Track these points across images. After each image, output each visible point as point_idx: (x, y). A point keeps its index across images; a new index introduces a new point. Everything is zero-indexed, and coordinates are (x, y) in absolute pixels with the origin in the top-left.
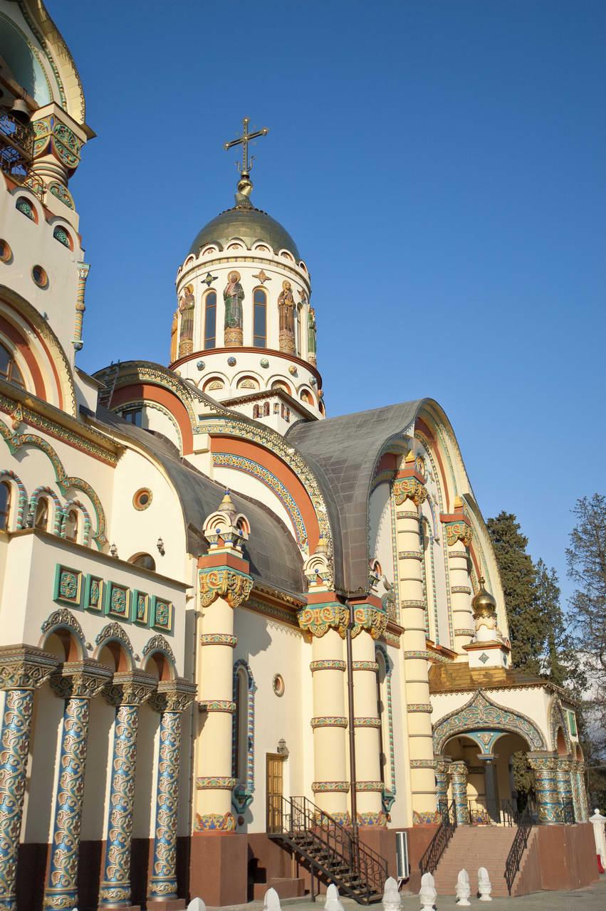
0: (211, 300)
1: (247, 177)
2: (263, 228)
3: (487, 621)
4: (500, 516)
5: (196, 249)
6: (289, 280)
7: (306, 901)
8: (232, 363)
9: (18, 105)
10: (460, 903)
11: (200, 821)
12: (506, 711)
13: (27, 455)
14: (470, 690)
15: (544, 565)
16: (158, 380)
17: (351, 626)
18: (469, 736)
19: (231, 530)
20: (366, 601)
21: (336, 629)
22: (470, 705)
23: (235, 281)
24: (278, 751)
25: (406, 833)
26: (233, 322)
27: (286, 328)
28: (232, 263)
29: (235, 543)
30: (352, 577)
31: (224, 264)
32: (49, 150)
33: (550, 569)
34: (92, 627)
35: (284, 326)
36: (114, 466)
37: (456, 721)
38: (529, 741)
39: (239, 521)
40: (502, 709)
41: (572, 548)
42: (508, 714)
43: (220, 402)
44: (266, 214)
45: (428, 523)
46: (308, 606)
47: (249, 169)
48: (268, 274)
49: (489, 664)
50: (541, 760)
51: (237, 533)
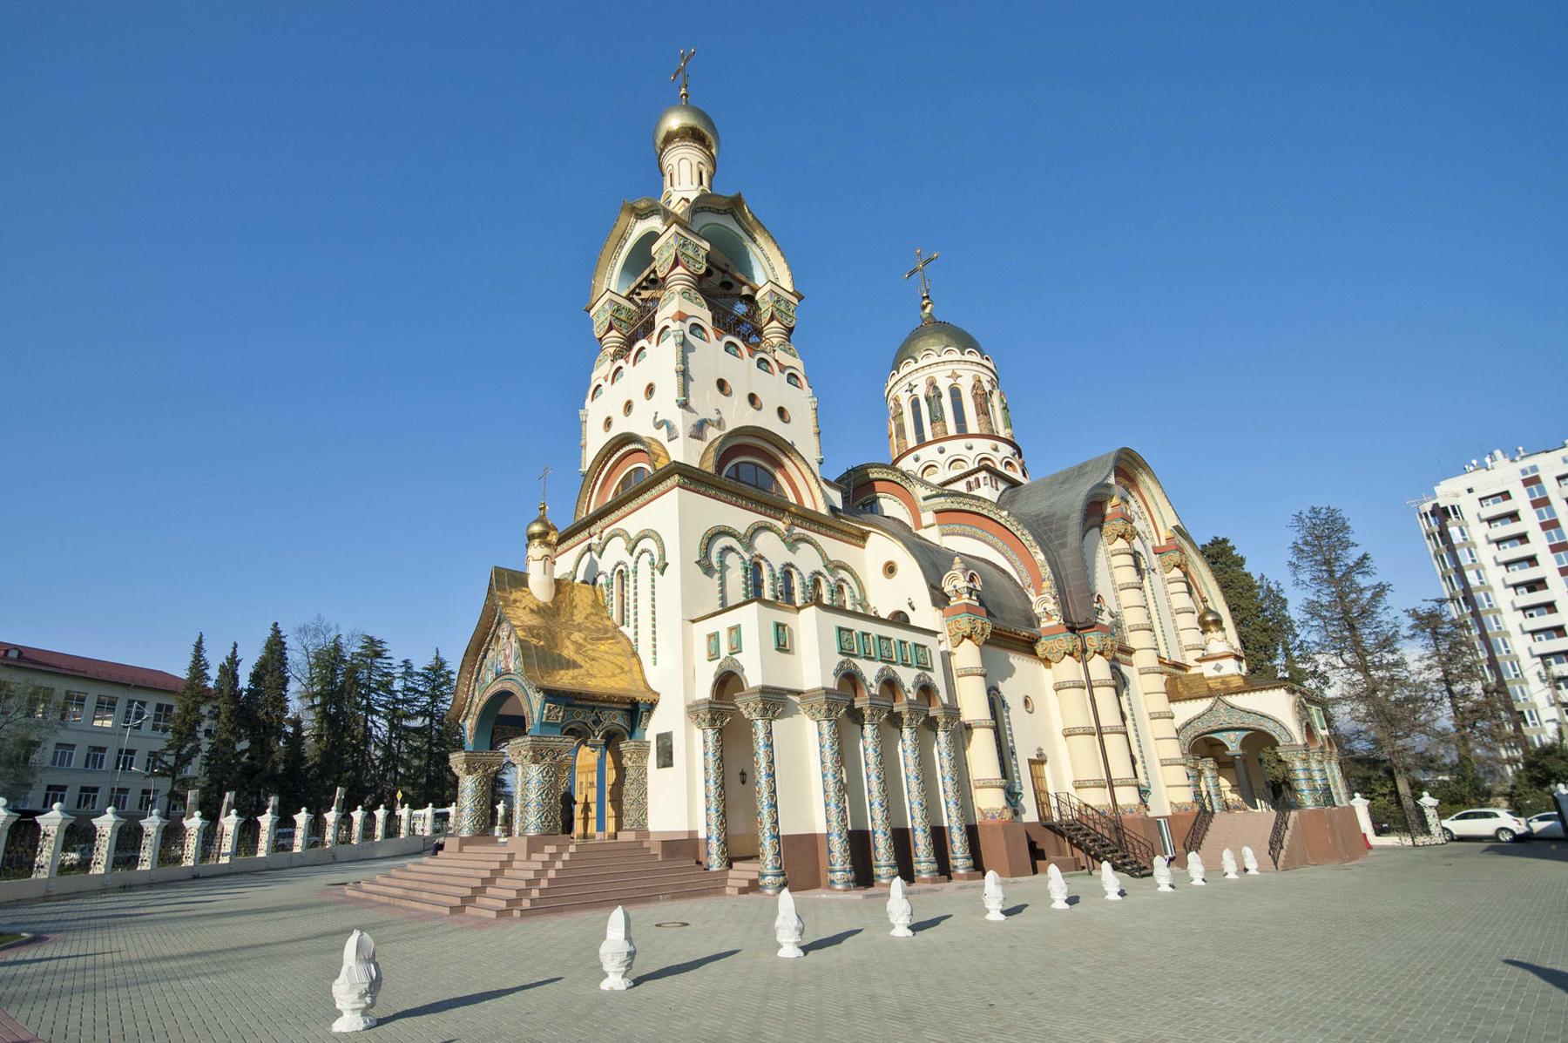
0: (915, 404)
1: (928, 297)
3: (1215, 635)
5: (896, 366)
8: (942, 451)
9: (745, 291)
11: (982, 812)
16: (885, 476)
17: (1085, 651)
18: (1213, 736)
19: (965, 584)
21: (1071, 654)
22: (1211, 709)
23: (932, 385)
26: (937, 418)
28: (928, 370)
29: (971, 594)
31: (921, 373)
32: (772, 318)
34: (870, 671)
36: (864, 547)
41: (1294, 560)
47: (928, 291)
48: (959, 373)
49: (1223, 673)
51: (971, 586)
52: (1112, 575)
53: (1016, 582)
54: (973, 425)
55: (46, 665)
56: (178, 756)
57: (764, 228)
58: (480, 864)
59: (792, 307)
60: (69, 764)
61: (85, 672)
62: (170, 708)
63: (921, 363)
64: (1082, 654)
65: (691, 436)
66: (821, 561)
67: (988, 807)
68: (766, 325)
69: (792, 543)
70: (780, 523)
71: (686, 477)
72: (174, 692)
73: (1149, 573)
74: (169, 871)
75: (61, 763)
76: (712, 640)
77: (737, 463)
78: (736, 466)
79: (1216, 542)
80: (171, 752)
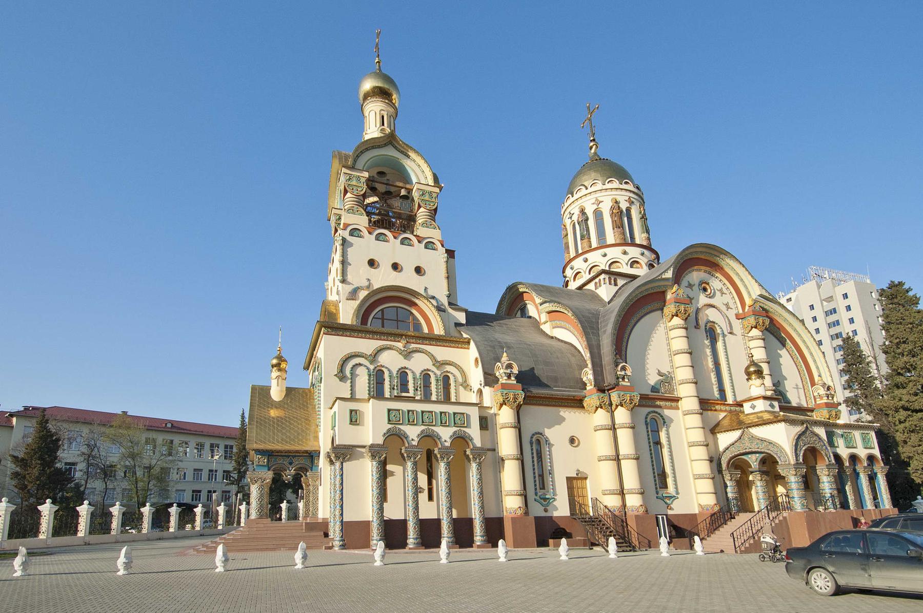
1: (594, 140)
2: (595, 171)
3: (755, 381)
4: (889, 285)
6: (614, 196)
7: (587, 549)
8: (586, 260)
9: (403, 192)
13: (413, 357)
19: (824, 392)
20: (615, 390)
23: (583, 212)
25: (665, 516)
26: (586, 236)
27: (616, 227)
29: (828, 397)
30: (608, 377)
35: (615, 226)
36: (469, 349)
40: (758, 439)
43: (576, 289)
44: (607, 159)
45: (717, 324)
46: (586, 398)
48: (600, 199)
49: (756, 410)
50: (786, 470)
51: (828, 393)
52: (669, 344)
53: (583, 357)
54: (611, 238)
55: (184, 430)
56: (239, 472)
57: (414, 150)
59: (434, 195)
60: (201, 479)
61: (202, 432)
62: (231, 447)
63: (576, 197)
64: (610, 407)
65: (347, 299)
66: (431, 362)
67: (705, 504)
68: (417, 212)
69: (407, 355)
70: (399, 344)
71: (328, 327)
72: (235, 439)
73: (724, 336)
74: (182, 533)
75: (198, 479)
76: (484, 426)
77: (382, 309)
78: (382, 310)
79: (892, 286)
80: (235, 472)
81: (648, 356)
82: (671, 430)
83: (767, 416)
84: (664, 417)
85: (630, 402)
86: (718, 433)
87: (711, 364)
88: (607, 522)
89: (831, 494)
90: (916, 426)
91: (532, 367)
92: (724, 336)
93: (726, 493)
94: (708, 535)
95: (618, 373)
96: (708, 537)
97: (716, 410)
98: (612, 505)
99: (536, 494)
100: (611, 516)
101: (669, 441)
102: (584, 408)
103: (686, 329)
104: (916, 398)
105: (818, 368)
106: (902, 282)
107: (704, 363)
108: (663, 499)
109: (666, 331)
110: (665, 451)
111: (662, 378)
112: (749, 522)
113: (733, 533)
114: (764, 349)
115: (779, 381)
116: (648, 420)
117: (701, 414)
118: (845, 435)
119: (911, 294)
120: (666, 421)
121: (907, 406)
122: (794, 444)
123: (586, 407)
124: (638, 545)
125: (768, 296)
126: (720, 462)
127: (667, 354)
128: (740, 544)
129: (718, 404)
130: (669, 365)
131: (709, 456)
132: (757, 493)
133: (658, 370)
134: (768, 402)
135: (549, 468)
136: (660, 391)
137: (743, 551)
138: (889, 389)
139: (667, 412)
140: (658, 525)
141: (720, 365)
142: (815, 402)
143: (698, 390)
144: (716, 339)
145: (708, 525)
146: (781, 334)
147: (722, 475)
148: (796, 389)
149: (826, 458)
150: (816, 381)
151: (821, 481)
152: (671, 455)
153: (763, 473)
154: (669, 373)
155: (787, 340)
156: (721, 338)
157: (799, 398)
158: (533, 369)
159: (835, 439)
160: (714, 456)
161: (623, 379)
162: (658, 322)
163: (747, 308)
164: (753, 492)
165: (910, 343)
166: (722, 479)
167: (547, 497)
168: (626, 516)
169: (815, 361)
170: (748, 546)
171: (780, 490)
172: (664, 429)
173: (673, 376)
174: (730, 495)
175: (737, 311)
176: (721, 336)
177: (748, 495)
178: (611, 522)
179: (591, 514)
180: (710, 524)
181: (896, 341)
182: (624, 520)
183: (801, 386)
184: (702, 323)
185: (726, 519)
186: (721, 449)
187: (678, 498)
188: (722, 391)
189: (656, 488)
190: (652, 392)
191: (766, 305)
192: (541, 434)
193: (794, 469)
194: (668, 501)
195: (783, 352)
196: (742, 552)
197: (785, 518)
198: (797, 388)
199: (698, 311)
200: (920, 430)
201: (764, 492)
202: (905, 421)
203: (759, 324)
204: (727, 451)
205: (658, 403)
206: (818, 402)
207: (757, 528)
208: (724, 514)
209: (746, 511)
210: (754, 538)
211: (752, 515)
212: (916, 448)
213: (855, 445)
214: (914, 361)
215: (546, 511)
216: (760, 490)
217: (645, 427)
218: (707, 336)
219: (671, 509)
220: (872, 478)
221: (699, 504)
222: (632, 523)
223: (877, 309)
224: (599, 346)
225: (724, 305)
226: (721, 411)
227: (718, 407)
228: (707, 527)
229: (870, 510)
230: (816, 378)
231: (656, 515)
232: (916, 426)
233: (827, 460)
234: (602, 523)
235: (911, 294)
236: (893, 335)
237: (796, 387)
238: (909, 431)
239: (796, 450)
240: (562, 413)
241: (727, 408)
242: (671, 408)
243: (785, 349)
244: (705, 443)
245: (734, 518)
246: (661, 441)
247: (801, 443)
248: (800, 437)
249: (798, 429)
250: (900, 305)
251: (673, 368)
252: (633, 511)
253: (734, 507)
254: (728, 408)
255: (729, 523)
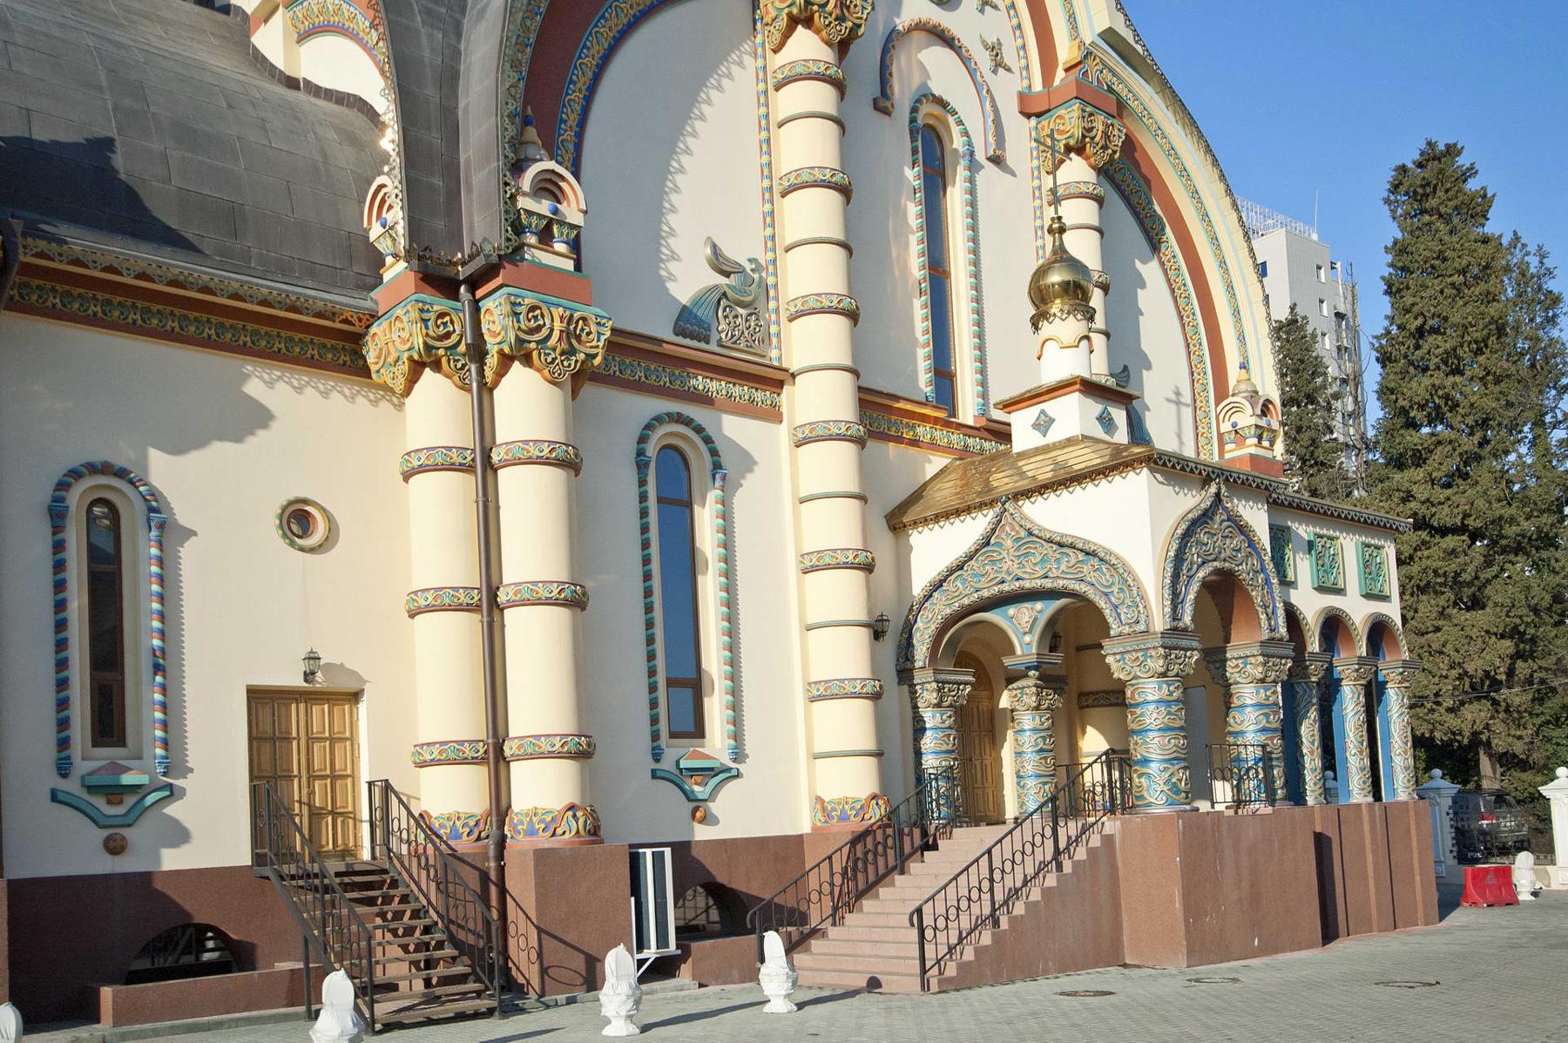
3: (1064, 327)
4: (1422, 154)
10: (608, 1031)
12: (1061, 545)
14: (981, 506)
15: (1524, 245)
19: (1253, 421)
22: (986, 542)
24: (306, 681)
25: (668, 851)
29: (1260, 438)
30: (476, 220)
33: (1532, 248)
37: (959, 585)
38: (1107, 612)
39: (1264, 405)
40: (1050, 541)
42: (1064, 550)
45: (954, 113)
49: (1056, 434)
50: (1135, 655)
51: (1263, 423)
58: (881, 920)
73: (974, 167)
81: (679, 178)
82: (739, 501)
83: (1083, 458)
84: (719, 445)
85: (564, 346)
86: (915, 524)
87: (915, 264)
88: (417, 884)
89: (1264, 747)
90: (1435, 571)
91: (99, 131)
92: (974, 167)
93: (918, 754)
94: (833, 915)
95: (520, 205)
96: (834, 924)
97: (915, 443)
98: (449, 809)
99: (64, 769)
100: (431, 862)
101: (728, 545)
102: (365, 372)
103: (839, 85)
104: (1448, 492)
105: (1241, 339)
106: (1455, 144)
107: (894, 254)
108: (678, 779)
109: (762, 86)
110: (709, 587)
111: (722, 280)
112: (984, 861)
113: (919, 911)
114: (1096, 235)
115: (1125, 368)
116: (651, 450)
117: (860, 442)
118: (1319, 544)
119: (1473, 185)
120: (725, 459)
121: (1424, 517)
122: (1172, 554)
123: (373, 368)
124: (535, 982)
125: (1131, 41)
126: (910, 636)
127: (757, 184)
128: (943, 950)
129: (924, 418)
130: (759, 233)
131: (870, 611)
132: (1019, 754)
133: (714, 246)
134: (1095, 407)
135: (156, 642)
136: (714, 337)
137: (950, 980)
138: (1372, 479)
139: (734, 429)
140: (636, 888)
141: (947, 275)
142: (1221, 452)
143: (857, 346)
144: (943, 176)
145: (838, 880)
146: (1150, 203)
147: (912, 686)
148: (1173, 407)
149: (1263, 617)
150: (1232, 382)
151: (1236, 702)
152: (731, 603)
153: (1050, 680)
154: (758, 268)
155: (1168, 230)
156: (961, 173)
157: (1179, 436)
158: (107, 144)
159: (1289, 554)
160: (888, 614)
161: (546, 237)
162: (734, 46)
163: (1060, 74)
164: (1007, 753)
165: (1448, 331)
166: (908, 700)
167: (127, 779)
168: (500, 856)
169: (1236, 313)
170: (972, 958)
171: (1093, 742)
172: (713, 495)
173: (771, 280)
174: (930, 762)
175: (1025, 83)
176: (963, 163)
177: (987, 762)
178: (433, 885)
179: (366, 855)
180: (844, 873)
181: (1414, 325)
182: (493, 876)
183: (1187, 398)
184: (902, 93)
185: (907, 849)
186: (919, 583)
187: (738, 776)
188: (944, 375)
189: (655, 736)
190: (677, 334)
191: (1121, 81)
192: (122, 473)
193: (1161, 651)
194: (697, 788)
195: (1150, 270)
196: (947, 986)
197: (1108, 840)
198: (1178, 403)
199: (892, 40)
200: (1444, 584)
201: (1041, 750)
202: (1411, 558)
203: (1093, 138)
204: (936, 594)
205: (699, 382)
206: (1227, 456)
207: (1009, 883)
208: (901, 833)
209: (976, 821)
210: (996, 923)
211: (997, 832)
212: (1429, 636)
213: (1341, 585)
214: (1454, 386)
215: (115, 847)
216: (1029, 741)
217: (632, 475)
218: (914, 152)
219: (708, 819)
220: (1373, 694)
221: (820, 800)
222: (521, 884)
223: (1325, 313)
224: (450, 78)
225: (986, 46)
226: (934, 446)
227: (924, 432)
228: (832, 885)
229: (1358, 806)
230: (1233, 373)
231: (631, 846)
232: (1435, 571)
233: (1264, 623)
234: (401, 890)
235: (1473, 185)
236: (1413, 305)
237: (1173, 397)
238: (1418, 586)
239: (1176, 576)
240: (255, 387)
241: (954, 438)
242: (749, 410)
243: (1155, 264)
244: (861, 559)
245: (935, 847)
246: (698, 544)
247: (1193, 553)
248: (1197, 523)
249: (1190, 501)
250: (1441, 216)
251: (774, 250)
252: (531, 832)
253: (938, 805)
254: (957, 439)
255: (914, 866)
